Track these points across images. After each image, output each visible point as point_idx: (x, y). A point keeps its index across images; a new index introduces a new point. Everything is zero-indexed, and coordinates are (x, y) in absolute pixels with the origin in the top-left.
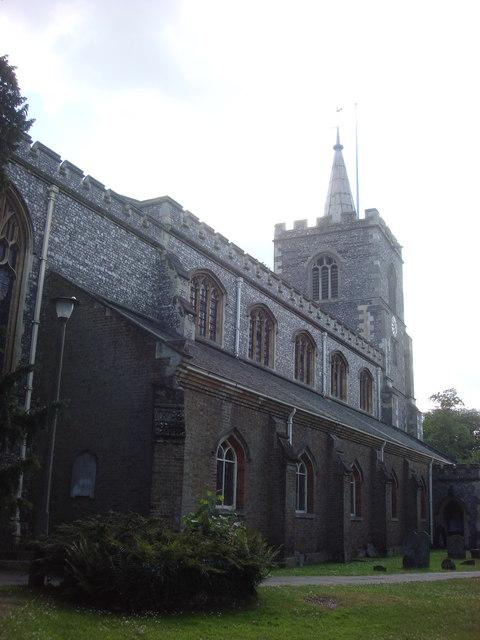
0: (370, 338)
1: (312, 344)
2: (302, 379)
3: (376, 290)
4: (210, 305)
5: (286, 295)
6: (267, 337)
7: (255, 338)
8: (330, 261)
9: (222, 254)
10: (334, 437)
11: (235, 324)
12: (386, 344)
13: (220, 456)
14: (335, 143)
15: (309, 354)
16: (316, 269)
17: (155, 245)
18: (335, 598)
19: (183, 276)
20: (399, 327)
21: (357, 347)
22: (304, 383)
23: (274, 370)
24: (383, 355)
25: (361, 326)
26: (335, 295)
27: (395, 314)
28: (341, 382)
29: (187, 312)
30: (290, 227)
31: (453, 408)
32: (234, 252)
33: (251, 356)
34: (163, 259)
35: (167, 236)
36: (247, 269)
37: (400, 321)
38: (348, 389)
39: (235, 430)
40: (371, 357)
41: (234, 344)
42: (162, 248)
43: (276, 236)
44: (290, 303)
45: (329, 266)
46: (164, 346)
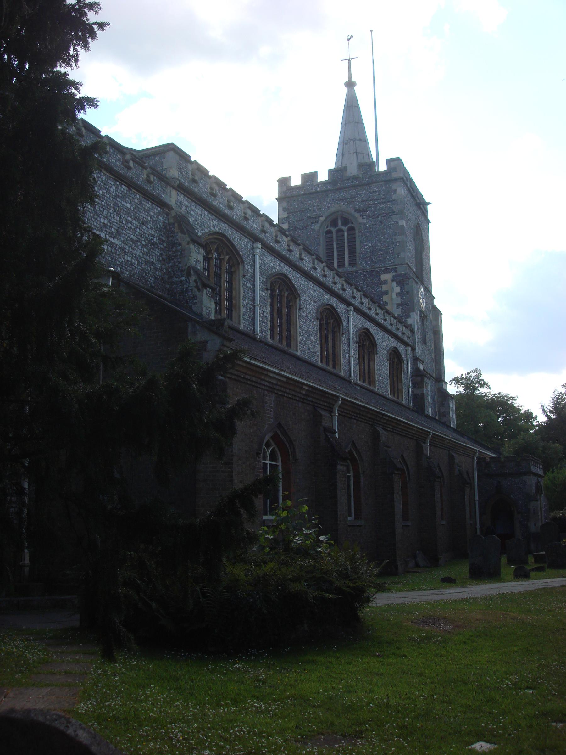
0: (397, 312)
1: (338, 322)
2: (327, 364)
3: (402, 255)
4: (225, 277)
5: (307, 263)
6: (289, 315)
7: (276, 315)
8: (346, 221)
9: (236, 214)
10: (379, 429)
11: (254, 300)
12: (414, 319)
13: (264, 459)
14: (347, 80)
15: (334, 332)
16: (329, 232)
17: (162, 204)
18: (445, 618)
19: (195, 241)
20: (427, 298)
21: (386, 324)
22: (329, 368)
23: (298, 353)
24: (413, 332)
25: (385, 298)
26: (353, 262)
27: (422, 284)
28: (369, 365)
29: (205, 286)
31: (477, 392)
32: (249, 212)
33: (272, 337)
34: (171, 221)
35: (174, 193)
36: (264, 232)
37: (428, 291)
38: (377, 372)
39: (280, 425)
40: (400, 334)
41: (254, 324)
42: (170, 208)
43: (280, 192)
44: (312, 272)
45: (345, 228)
46: (198, 327)
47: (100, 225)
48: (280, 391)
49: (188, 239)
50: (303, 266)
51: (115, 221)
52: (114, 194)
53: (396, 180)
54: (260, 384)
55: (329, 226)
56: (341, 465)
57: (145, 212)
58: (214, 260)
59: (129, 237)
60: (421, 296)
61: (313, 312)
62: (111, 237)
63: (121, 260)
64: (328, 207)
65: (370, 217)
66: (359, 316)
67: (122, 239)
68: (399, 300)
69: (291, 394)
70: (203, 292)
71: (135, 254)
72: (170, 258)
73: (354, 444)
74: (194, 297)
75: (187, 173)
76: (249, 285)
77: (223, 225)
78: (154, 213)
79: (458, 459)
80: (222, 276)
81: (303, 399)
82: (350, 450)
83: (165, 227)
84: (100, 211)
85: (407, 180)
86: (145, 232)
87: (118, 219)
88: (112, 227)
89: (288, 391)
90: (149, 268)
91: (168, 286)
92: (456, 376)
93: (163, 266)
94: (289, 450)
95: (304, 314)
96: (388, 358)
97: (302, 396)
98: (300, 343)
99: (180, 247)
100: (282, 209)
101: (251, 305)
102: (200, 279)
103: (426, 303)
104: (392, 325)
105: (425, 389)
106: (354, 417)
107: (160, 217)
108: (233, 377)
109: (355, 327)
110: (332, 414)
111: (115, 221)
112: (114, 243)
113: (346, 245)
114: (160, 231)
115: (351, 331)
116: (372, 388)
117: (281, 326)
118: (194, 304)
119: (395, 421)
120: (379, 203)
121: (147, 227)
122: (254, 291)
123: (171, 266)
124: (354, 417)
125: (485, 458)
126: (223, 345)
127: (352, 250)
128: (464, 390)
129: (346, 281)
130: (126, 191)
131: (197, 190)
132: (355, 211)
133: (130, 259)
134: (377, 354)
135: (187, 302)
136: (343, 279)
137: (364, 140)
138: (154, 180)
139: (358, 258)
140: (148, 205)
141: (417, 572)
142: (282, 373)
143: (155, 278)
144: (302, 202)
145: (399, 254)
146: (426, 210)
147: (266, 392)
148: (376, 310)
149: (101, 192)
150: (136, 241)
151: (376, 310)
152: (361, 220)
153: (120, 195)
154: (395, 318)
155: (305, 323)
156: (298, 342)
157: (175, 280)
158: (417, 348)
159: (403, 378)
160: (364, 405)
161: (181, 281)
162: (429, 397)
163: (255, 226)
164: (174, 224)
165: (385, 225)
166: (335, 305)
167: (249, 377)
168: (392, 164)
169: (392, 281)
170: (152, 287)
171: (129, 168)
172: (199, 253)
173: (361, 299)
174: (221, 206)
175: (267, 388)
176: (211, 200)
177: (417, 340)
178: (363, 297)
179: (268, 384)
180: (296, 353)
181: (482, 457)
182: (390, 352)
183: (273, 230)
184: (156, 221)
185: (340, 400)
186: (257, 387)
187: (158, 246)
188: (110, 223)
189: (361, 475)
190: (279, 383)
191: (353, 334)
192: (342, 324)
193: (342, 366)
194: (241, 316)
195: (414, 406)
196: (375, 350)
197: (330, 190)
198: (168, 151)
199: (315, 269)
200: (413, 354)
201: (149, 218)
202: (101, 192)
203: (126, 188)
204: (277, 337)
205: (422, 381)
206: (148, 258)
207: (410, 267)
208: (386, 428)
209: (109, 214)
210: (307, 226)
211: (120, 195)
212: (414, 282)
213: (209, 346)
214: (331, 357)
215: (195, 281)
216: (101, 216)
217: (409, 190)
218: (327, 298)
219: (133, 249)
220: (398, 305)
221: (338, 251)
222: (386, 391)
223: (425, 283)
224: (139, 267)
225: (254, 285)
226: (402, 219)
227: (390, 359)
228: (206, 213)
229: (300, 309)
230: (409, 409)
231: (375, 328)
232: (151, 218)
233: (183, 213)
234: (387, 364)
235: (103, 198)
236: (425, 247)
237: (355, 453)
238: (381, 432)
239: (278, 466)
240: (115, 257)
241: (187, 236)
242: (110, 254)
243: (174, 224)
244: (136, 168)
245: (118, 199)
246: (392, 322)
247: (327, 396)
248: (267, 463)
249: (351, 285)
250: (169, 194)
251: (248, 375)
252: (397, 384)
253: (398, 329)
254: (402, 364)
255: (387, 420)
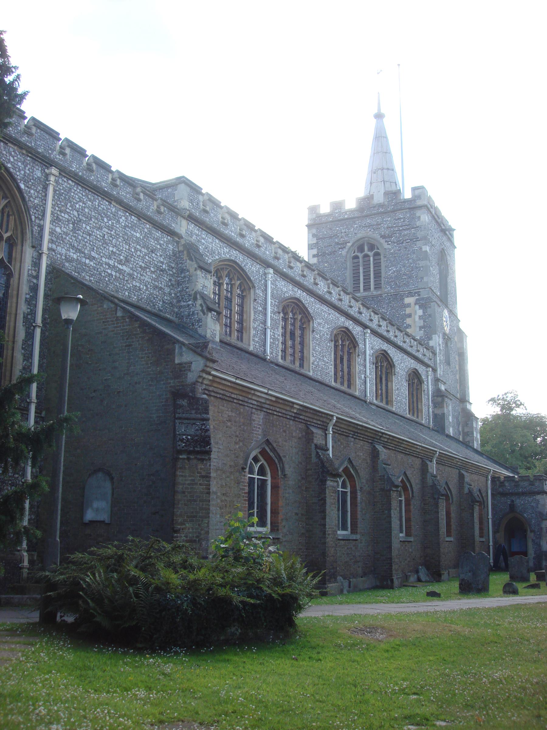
1: (354, 344)
3: (425, 279)
4: (236, 300)
5: (322, 288)
6: (302, 336)
8: (372, 247)
9: (248, 242)
10: (379, 448)
11: (265, 322)
12: (437, 341)
14: (377, 112)
16: (356, 257)
17: (171, 233)
18: (383, 628)
20: (452, 321)
21: (405, 346)
22: (344, 388)
24: (434, 354)
26: (378, 286)
27: (447, 306)
29: (210, 310)
30: (325, 209)
32: (262, 240)
33: (284, 358)
34: (181, 248)
35: (184, 222)
36: (277, 258)
37: (453, 314)
38: (395, 393)
39: (268, 442)
41: (264, 345)
42: (180, 237)
44: (327, 296)
45: (371, 254)
47: (109, 253)
48: (270, 409)
49: (196, 266)
50: (318, 290)
51: (124, 249)
52: (123, 224)
53: (420, 207)
54: (247, 402)
55: (356, 251)
56: (331, 481)
57: (154, 240)
58: (225, 285)
59: (138, 264)
60: (444, 319)
61: (327, 334)
62: (120, 264)
63: (129, 286)
64: (355, 233)
65: (394, 243)
66: (377, 339)
67: (131, 266)
68: (421, 323)
69: (281, 413)
70: (207, 315)
71: (144, 280)
72: (179, 284)
73: (350, 461)
74: (199, 321)
75: (198, 204)
76: (261, 309)
77: (234, 252)
78: (164, 241)
79: (468, 478)
80: (233, 300)
81: (294, 417)
82: (347, 467)
83: (174, 255)
84: (109, 240)
85: (432, 208)
86: (155, 259)
87: (127, 247)
88: (121, 255)
89: (278, 410)
90: (157, 293)
91: (176, 310)
92: (493, 397)
93: (172, 291)
94: (278, 466)
95: (318, 336)
96: (407, 379)
97: (293, 415)
98: (313, 364)
99: (188, 273)
100: (311, 235)
101: (262, 327)
102: (205, 303)
103: (450, 325)
104: (411, 347)
105: (445, 409)
106: (351, 436)
107: (170, 246)
108: (218, 396)
109: (372, 349)
110: (327, 432)
111: (124, 249)
112: (122, 270)
113: (372, 269)
114: (170, 258)
115: (368, 352)
116: (389, 407)
117: (293, 347)
118: (199, 327)
119: (397, 440)
120: (404, 230)
121: (156, 255)
122: (265, 315)
123: (180, 291)
124: (351, 436)
125: (499, 477)
126: (206, 366)
127: (378, 275)
128: (501, 410)
129: (362, 304)
130: (135, 222)
131: (208, 219)
132: (381, 237)
133: (138, 285)
134: (395, 374)
135: (193, 325)
136: (360, 302)
137: (391, 169)
138: (164, 211)
139: (383, 282)
140: (158, 235)
141: (414, 586)
142: (270, 392)
143: (164, 302)
144: (331, 229)
145: (422, 278)
146: (452, 235)
147: (254, 410)
148: (395, 333)
149: (110, 222)
150: (145, 267)
151: (395, 333)
152: (386, 246)
153: (130, 225)
154: (415, 340)
155: (319, 345)
156: (311, 363)
157: (183, 304)
158: (438, 369)
159: (423, 399)
160: (361, 423)
161: (188, 305)
162: (450, 418)
163: (268, 253)
164: (183, 251)
165: (409, 250)
166: (350, 328)
167: (235, 396)
168: (417, 192)
169: (415, 304)
170: (161, 311)
171: (139, 200)
172: (206, 279)
173: (379, 322)
174: (233, 234)
175: (255, 407)
176: (222, 229)
177: (438, 361)
178: (381, 320)
179: (255, 403)
180: (308, 373)
181: (497, 476)
182: (409, 373)
183: (286, 256)
184: (166, 249)
185: (335, 418)
186: (244, 405)
187: (167, 272)
188: (119, 251)
189: (358, 491)
190: (268, 402)
191: (369, 355)
192: (358, 345)
193: (357, 386)
194: (251, 338)
195: (435, 426)
196: (393, 371)
197: (358, 217)
198: (180, 183)
199: (330, 293)
200: (435, 375)
201: (159, 247)
202: (110, 222)
203: (136, 219)
204: (289, 358)
205: (443, 401)
206: (156, 283)
207: (433, 291)
208: (388, 447)
209: (118, 243)
210: (335, 251)
211: (130, 225)
212: (436, 305)
213: (193, 367)
214: (346, 378)
215: (201, 305)
216: (109, 245)
217: (433, 217)
218: (342, 321)
219: (142, 275)
220: (421, 328)
221: (364, 276)
222: (405, 410)
223: (450, 306)
224: (147, 292)
225: (265, 309)
226: (425, 244)
227: (409, 379)
228: (217, 241)
229: (313, 331)
230: (429, 428)
231: (394, 349)
232: (160, 246)
233: (193, 241)
234: (406, 384)
235: (112, 228)
236: (450, 271)
237: (351, 470)
238: (380, 450)
239: (266, 480)
240: (124, 283)
241: (194, 262)
242: (118, 280)
243: (183, 251)
244: (146, 200)
245: (127, 229)
246: (412, 344)
247: (320, 414)
248: (255, 478)
249: (368, 308)
250: (179, 223)
251: (235, 394)
252: (417, 404)
253: (418, 351)
254: (423, 385)
255: (388, 439)
